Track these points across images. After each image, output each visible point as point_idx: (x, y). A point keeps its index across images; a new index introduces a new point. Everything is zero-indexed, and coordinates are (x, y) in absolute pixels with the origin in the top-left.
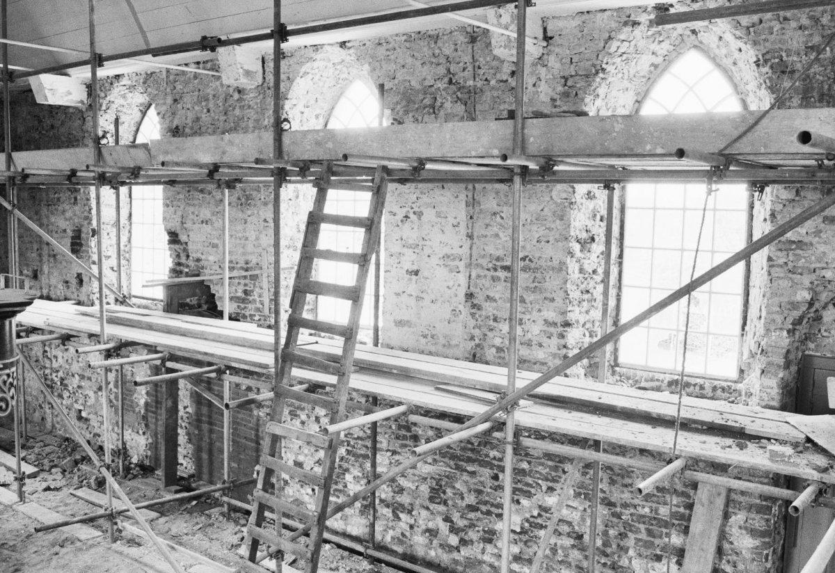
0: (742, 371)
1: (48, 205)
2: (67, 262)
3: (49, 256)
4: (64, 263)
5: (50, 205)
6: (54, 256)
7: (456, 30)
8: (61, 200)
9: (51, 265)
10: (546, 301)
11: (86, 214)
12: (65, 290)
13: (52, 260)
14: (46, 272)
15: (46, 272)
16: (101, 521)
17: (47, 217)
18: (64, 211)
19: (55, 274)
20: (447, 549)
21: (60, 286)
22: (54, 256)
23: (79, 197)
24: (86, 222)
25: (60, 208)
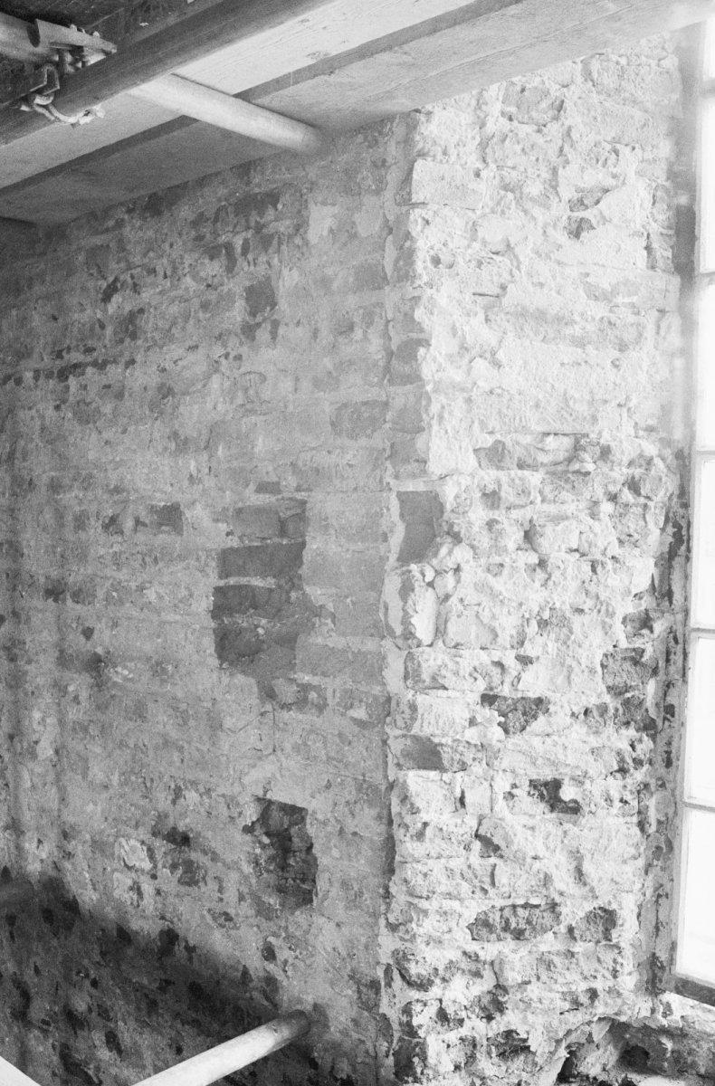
0: (193, 504)
1: (63, 375)
2: (183, 719)
3: (64, 660)
4: (162, 720)
5: (76, 368)
6: (96, 664)
7: (263, 628)
8: (148, 323)
9: (73, 714)
10: (519, 552)
11: (356, 388)
12: (169, 880)
13: (79, 683)
14: (46, 750)
15: (46, 750)
16: (496, 969)
17: (53, 438)
18: (166, 391)
19: (97, 772)
20: (650, 646)
21: (133, 850)
22: (96, 664)
23: (288, 281)
24: (352, 453)
25: (142, 377)
